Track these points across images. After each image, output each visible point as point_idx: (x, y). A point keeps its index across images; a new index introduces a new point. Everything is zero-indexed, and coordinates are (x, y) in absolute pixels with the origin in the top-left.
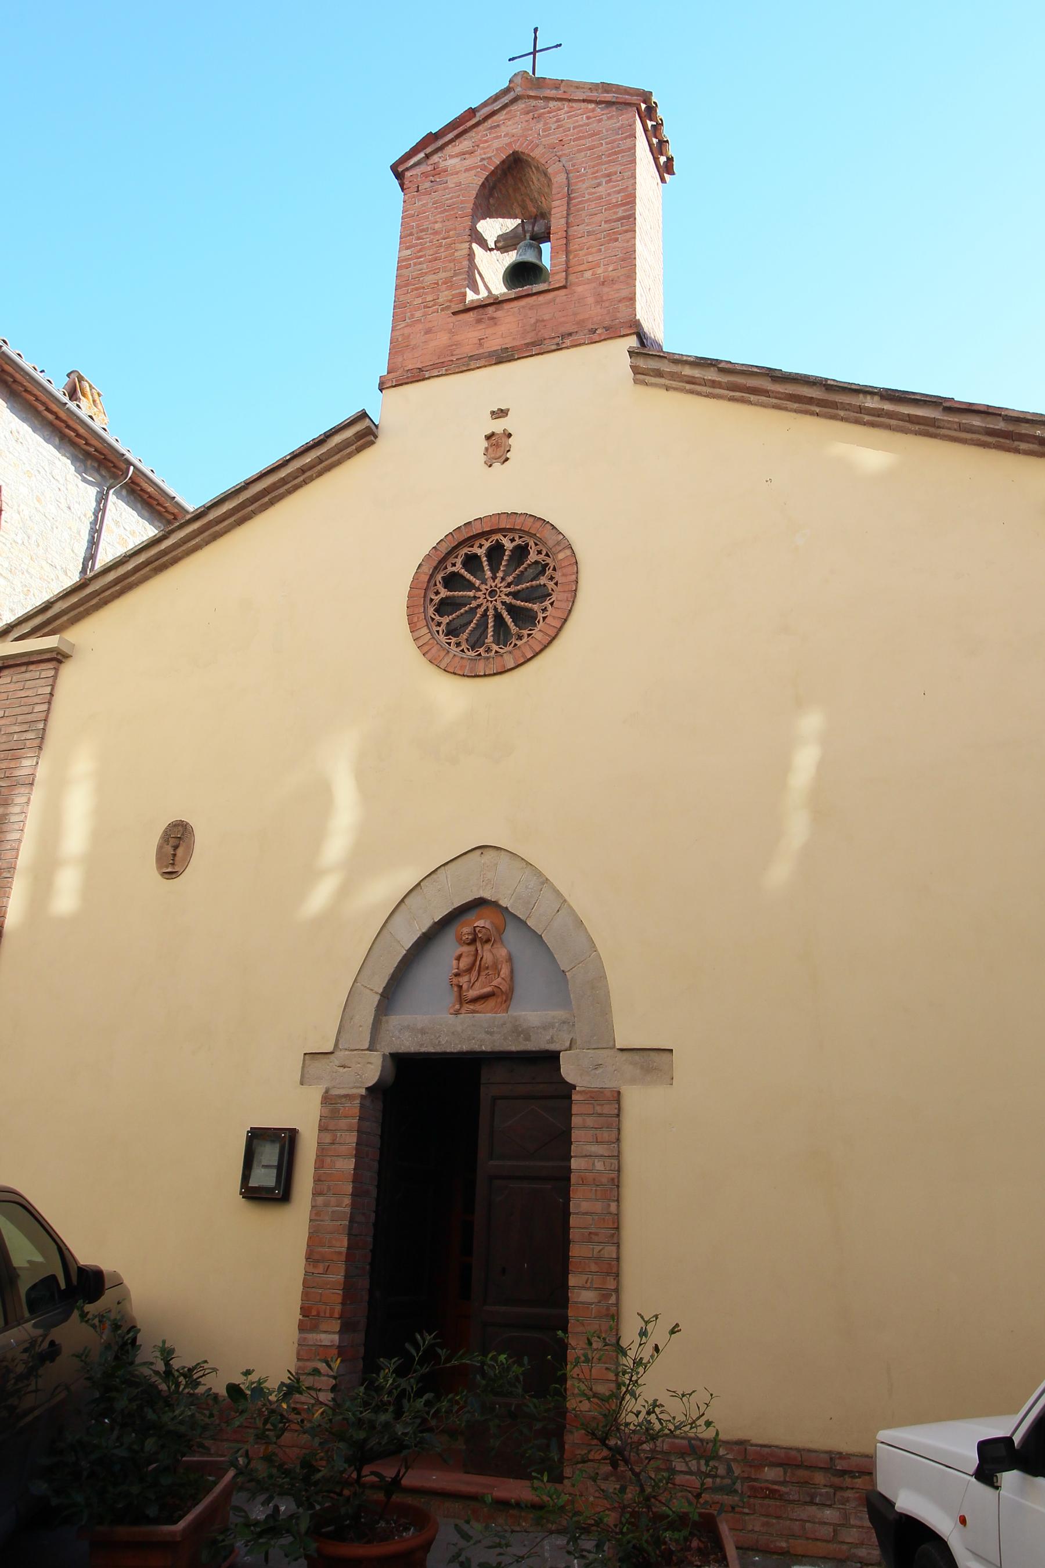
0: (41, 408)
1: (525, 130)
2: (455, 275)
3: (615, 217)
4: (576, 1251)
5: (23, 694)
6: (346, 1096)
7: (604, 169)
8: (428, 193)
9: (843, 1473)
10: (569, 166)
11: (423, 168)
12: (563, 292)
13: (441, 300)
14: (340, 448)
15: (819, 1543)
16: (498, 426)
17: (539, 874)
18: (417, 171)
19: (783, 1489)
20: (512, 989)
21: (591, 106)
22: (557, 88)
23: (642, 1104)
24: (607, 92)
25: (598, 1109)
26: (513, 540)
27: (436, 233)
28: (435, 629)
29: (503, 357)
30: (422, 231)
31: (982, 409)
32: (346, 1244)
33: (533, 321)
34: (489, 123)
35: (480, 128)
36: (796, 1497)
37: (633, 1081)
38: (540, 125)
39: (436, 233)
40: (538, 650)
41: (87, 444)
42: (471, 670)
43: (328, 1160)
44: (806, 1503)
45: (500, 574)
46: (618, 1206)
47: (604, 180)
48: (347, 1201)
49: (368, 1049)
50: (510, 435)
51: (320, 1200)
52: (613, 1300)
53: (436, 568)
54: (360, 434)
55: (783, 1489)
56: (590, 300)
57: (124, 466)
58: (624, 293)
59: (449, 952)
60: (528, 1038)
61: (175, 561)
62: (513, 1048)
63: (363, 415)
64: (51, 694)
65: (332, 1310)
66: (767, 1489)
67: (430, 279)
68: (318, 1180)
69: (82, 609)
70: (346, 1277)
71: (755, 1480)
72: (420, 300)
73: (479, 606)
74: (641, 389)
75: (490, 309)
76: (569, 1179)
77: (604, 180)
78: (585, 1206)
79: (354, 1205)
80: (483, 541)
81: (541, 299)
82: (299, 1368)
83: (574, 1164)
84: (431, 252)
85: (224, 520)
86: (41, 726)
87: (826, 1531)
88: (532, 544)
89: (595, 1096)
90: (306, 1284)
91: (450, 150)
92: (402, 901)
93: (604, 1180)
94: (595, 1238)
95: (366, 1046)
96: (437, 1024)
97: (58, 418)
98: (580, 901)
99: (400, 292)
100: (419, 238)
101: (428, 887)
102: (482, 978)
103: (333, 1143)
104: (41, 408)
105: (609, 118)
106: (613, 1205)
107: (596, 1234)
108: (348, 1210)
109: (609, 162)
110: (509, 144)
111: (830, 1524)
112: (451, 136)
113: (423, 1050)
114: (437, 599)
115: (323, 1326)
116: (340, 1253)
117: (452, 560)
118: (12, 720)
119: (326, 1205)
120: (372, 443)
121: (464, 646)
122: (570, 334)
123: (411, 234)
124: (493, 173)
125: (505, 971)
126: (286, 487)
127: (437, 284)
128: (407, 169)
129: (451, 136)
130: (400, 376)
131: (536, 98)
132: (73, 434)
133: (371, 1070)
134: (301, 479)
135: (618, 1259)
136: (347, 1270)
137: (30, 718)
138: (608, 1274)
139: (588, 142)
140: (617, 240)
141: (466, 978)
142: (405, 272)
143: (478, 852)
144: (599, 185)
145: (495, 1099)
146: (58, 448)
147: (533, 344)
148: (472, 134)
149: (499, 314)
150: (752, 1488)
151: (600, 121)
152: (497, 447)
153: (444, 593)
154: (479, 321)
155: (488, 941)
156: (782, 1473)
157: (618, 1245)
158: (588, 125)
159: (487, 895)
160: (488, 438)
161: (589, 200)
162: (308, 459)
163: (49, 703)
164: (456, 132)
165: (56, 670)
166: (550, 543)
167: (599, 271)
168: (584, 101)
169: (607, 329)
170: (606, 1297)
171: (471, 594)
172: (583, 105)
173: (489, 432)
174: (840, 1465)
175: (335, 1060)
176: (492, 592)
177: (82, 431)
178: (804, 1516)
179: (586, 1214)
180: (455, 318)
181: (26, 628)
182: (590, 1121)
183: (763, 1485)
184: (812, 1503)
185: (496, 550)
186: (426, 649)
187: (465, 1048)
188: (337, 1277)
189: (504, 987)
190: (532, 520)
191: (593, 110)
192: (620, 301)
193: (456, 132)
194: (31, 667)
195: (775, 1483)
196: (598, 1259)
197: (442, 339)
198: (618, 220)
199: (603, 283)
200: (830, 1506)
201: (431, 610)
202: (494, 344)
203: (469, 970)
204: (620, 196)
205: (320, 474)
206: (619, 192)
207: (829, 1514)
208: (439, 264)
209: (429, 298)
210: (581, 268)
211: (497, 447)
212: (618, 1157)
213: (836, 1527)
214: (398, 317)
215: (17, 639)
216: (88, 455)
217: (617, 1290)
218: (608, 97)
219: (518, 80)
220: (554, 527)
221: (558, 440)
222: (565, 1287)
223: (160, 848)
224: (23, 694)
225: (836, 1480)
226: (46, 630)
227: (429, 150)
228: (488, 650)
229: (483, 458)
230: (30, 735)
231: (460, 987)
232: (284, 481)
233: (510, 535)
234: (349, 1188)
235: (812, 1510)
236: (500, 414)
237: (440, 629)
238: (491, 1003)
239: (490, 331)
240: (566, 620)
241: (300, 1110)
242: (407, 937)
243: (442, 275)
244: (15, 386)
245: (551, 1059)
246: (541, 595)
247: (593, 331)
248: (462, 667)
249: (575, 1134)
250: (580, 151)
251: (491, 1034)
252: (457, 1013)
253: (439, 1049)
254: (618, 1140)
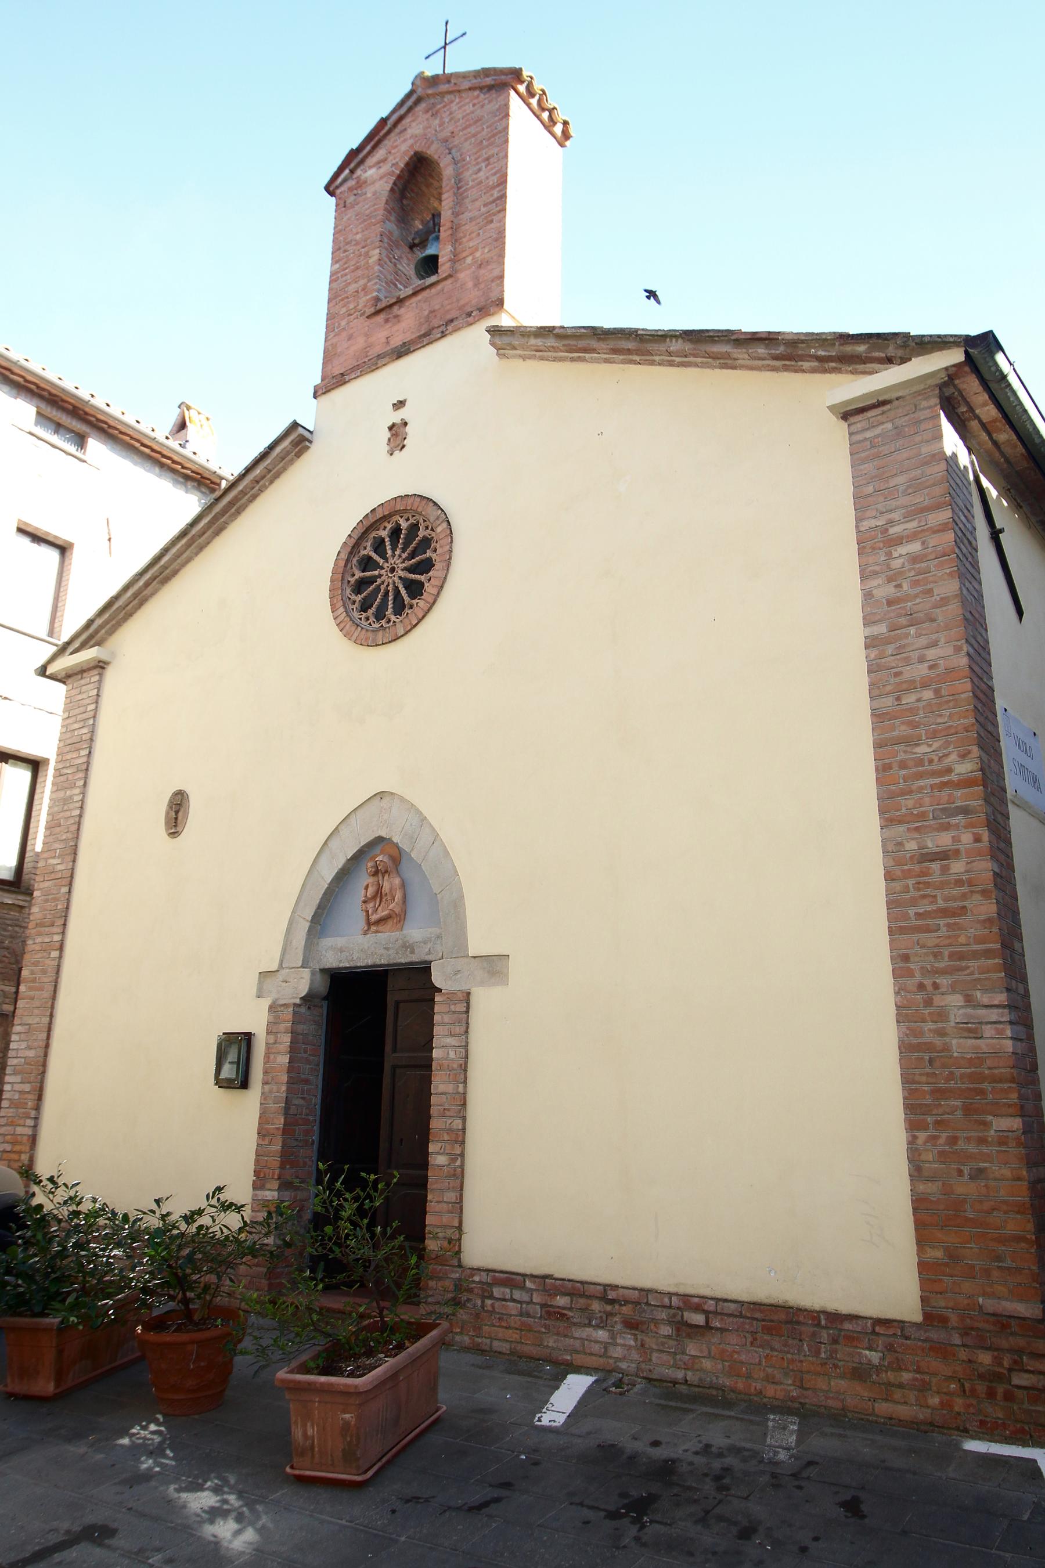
0: (137, 445)
1: (425, 128)
2: (369, 281)
3: (491, 199)
4: (435, 1124)
5: (80, 697)
6: (285, 1005)
7: (484, 154)
8: (352, 206)
9: (612, 1302)
10: (458, 157)
11: (351, 183)
12: (449, 281)
13: (360, 307)
14: (282, 458)
15: (594, 1358)
16: (396, 417)
17: (419, 813)
18: (342, 189)
19: (570, 1314)
20: (405, 912)
21: (476, 93)
22: (449, 82)
23: (488, 1004)
24: (487, 76)
25: (453, 1008)
26: (407, 520)
27: (357, 244)
28: (351, 607)
29: (402, 352)
30: (347, 244)
31: (764, 336)
32: (282, 1120)
33: (426, 313)
34: (400, 127)
35: (392, 134)
36: (578, 1320)
37: (482, 983)
38: (437, 122)
39: (357, 244)
40: (420, 616)
41: (183, 467)
42: (374, 640)
43: (272, 1057)
44: (585, 1325)
45: (397, 553)
46: (465, 1087)
47: (483, 165)
48: (284, 1088)
49: (302, 967)
50: (406, 424)
51: (267, 1087)
52: (458, 1163)
53: (351, 553)
54: (295, 442)
55: (570, 1314)
56: (470, 284)
57: (218, 481)
58: (496, 273)
59: (363, 883)
60: (412, 952)
61: (175, 573)
62: (403, 961)
63: (295, 425)
64: (98, 695)
65: (273, 1174)
66: (558, 1313)
67: (353, 287)
68: (265, 1072)
69: (114, 622)
70: (283, 1147)
71: (551, 1306)
72: (344, 310)
73: (383, 583)
74: (505, 361)
75: (396, 308)
76: (431, 1066)
77: (483, 165)
78: (442, 1088)
79: (288, 1090)
80: (386, 524)
81: (433, 291)
82: (253, 1217)
83: (436, 1053)
84: (353, 263)
85: (204, 533)
86: (91, 722)
87: (596, 1348)
88: (421, 521)
89: (451, 996)
90: (258, 1154)
91: (372, 160)
92: (326, 843)
93: (455, 1066)
94: (448, 1113)
95: (300, 965)
96: (355, 946)
97: (153, 450)
98: (449, 835)
99: (331, 304)
100: (345, 251)
101: (344, 831)
102: (383, 903)
103: (275, 1043)
104: (137, 445)
105: (490, 102)
106: (461, 1086)
107: (449, 1110)
108: (284, 1095)
109: (490, 145)
110: (411, 146)
111: (601, 1342)
112: (368, 148)
113: (341, 965)
114: (352, 580)
115: (268, 1186)
116: (278, 1129)
117: (364, 544)
118: (74, 719)
119: (271, 1092)
120: (308, 448)
121: (372, 619)
122: (452, 321)
123: (339, 249)
124: (399, 177)
125: (398, 896)
126: (246, 497)
127: (357, 292)
128: (337, 187)
129: (368, 148)
130: (332, 382)
131: (434, 95)
132: (169, 462)
133: (301, 984)
134: (257, 488)
135: (464, 1130)
136: (283, 1142)
137: (85, 716)
138: (456, 1142)
139: (472, 130)
140: (492, 221)
141: (371, 905)
142: (335, 285)
143: (378, 797)
144: (480, 170)
145: (397, 1004)
146: (159, 476)
147: (425, 335)
148: (386, 142)
149: (402, 311)
150: (548, 1312)
151: (482, 106)
152: (397, 434)
153: (359, 574)
154: (387, 321)
155: (386, 872)
156: (569, 1302)
157: (464, 1119)
158: (473, 112)
159: (384, 834)
160: (390, 428)
161: (473, 187)
162: (257, 471)
163: (97, 702)
164: (372, 143)
165: (101, 675)
166: (432, 519)
167: (478, 254)
168: (470, 89)
169: (480, 310)
170: (454, 1160)
171: (376, 573)
172: (470, 93)
173: (390, 424)
174: (611, 1295)
175: (280, 976)
176: (392, 569)
177: (176, 458)
178: (584, 1335)
179: (442, 1094)
180: (369, 321)
181: (76, 644)
182: (447, 1018)
183: (557, 1310)
184: (589, 1325)
185: (396, 532)
186: (342, 625)
187: (370, 962)
188: (277, 1147)
189: (397, 910)
190: (418, 500)
191: (478, 96)
192: (493, 281)
193: (372, 143)
194: (85, 675)
195: (564, 1308)
196: (449, 1131)
197: (360, 342)
198: (493, 202)
199: (480, 266)
200: (602, 1328)
201: (348, 591)
202: (397, 341)
203: (374, 898)
204: (495, 178)
205: (271, 482)
206: (495, 174)
207: (602, 1335)
208: (359, 272)
209: (352, 306)
210: (464, 254)
211: (397, 434)
212: (466, 1047)
213: (606, 1346)
214: (329, 329)
215: (72, 653)
216: (187, 478)
217: (462, 1155)
218: (489, 81)
219: (418, 82)
220: (435, 504)
221: (450, 421)
222: (426, 1154)
223: (167, 813)
224: (80, 697)
225: (609, 1308)
226: (92, 642)
227: (352, 165)
228: (389, 621)
229: (387, 448)
230: (85, 730)
231: (368, 912)
232: (243, 493)
233: (406, 516)
234: (285, 1078)
235: (589, 1330)
236: (400, 404)
237: (354, 607)
238: (390, 923)
239: (396, 328)
240: (442, 587)
241: (254, 1019)
242: (328, 873)
243: (362, 282)
244: (111, 431)
245: (425, 969)
246: (427, 566)
247: (469, 314)
248: (367, 639)
249: (437, 1030)
250: (466, 140)
251: (387, 949)
252: (365, 933)
253: (352, 964)
254: (467, 1032)
